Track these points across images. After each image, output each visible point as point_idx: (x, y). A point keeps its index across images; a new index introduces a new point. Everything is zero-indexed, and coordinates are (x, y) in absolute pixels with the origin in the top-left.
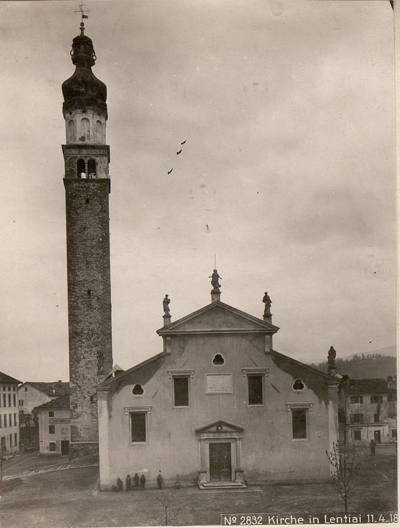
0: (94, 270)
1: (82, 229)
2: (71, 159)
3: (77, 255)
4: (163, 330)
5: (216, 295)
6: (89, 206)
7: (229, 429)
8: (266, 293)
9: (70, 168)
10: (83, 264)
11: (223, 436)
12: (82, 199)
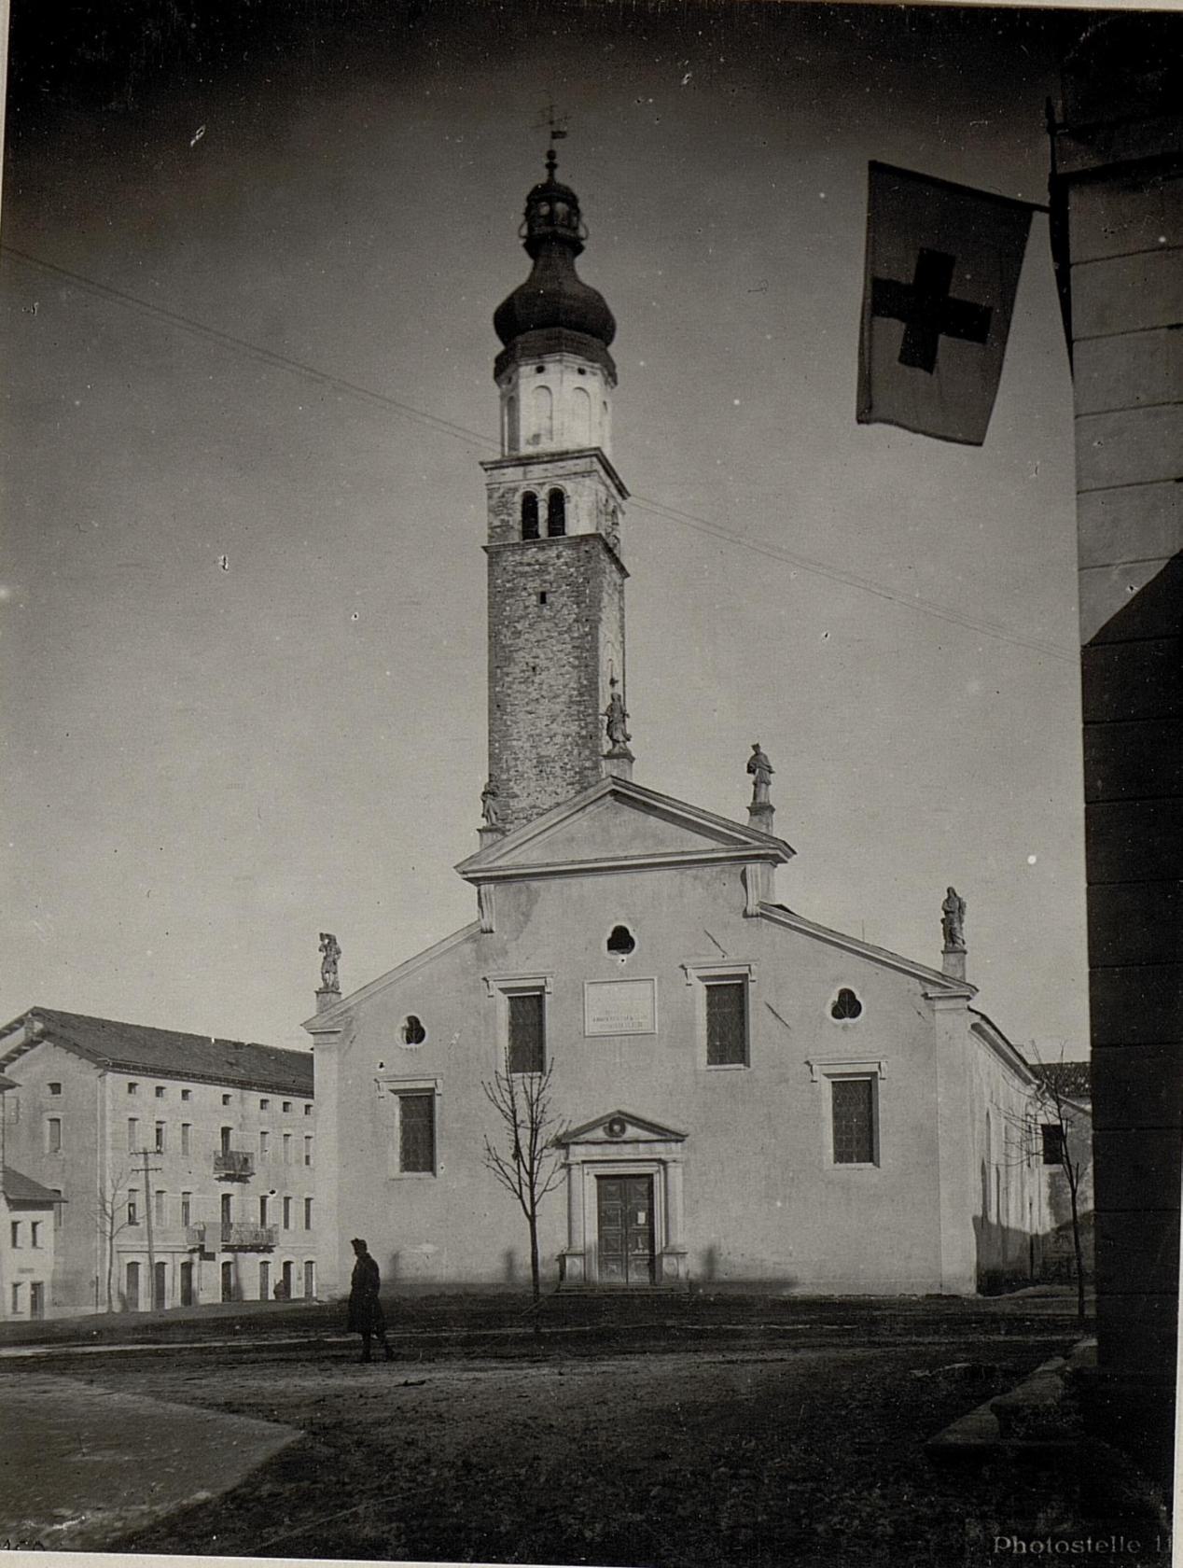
0: (555, 777)
1: (527, 673)
2: (503, 496)
3: (514, 743)
4: (470, 865)
5: (615, 761)
6: (547, 612)
7: (645, 1135)
8: (756, 747)
9: (502, 517)
10: (528, 764)
11: (627, 1152)
12: (530, 595)
